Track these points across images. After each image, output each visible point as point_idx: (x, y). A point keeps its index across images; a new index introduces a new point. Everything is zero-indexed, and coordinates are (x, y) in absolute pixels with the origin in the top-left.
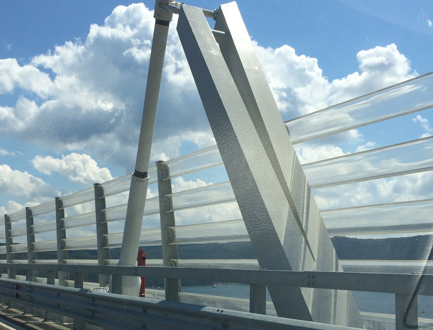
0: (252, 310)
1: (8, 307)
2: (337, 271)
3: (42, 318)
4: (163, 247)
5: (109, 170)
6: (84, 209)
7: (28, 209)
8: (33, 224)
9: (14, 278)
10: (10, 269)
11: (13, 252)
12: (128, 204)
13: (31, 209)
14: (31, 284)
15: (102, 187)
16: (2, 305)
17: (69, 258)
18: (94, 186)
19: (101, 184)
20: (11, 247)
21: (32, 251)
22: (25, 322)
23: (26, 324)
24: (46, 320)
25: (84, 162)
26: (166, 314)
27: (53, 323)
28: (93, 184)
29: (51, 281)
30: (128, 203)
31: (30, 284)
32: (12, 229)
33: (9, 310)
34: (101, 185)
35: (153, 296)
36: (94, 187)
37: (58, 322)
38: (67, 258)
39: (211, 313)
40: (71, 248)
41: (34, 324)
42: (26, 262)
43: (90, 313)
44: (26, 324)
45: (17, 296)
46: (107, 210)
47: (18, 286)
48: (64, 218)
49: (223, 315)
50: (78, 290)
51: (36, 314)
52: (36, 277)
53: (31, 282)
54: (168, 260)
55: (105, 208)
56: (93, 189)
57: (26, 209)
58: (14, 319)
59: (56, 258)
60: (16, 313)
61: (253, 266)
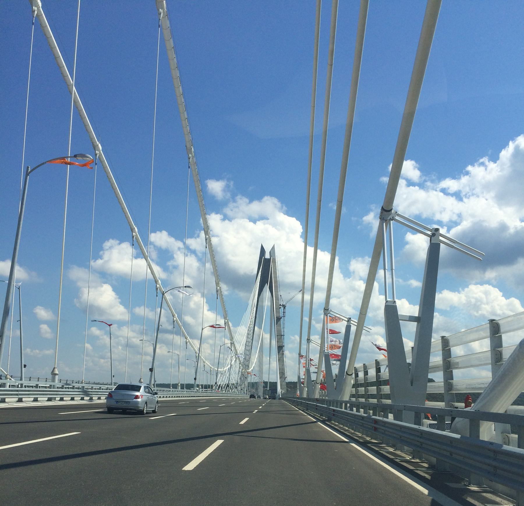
0: (356, 412)
2: (424, 406)
5: (518, 300)
6: (481, 346)
7: (494, 322)
8: (380, 372)
10: (414, 413)
12: (491, 350)
14: (383, 420)
16: (420, 463)
17: (457, 402)
19: (497, 320)
20: (380, 388)
21: (451, 392)
23: (415, 471)
24: (343, 426)
25: (486, 293)
26: (385, 424)
27: (477, 488)
28: (488, 320)
29: (358, 411)
30: (490, 350)
31: (419, 428)
32: (369, 374)
33: (469, 489)
34: (498, 321)
37: (486, 488)
38: (455, 402)
40: (461, 391)
41: (385, 452)
42: (441, 405)
43: (448, 454)
44: (415, 471)
46: (504, 349)
50: (365, 415)
51: (486, 488)
53: (420, 426)
55: (450, 358)
58: (402, 463)
60: (348, 432)
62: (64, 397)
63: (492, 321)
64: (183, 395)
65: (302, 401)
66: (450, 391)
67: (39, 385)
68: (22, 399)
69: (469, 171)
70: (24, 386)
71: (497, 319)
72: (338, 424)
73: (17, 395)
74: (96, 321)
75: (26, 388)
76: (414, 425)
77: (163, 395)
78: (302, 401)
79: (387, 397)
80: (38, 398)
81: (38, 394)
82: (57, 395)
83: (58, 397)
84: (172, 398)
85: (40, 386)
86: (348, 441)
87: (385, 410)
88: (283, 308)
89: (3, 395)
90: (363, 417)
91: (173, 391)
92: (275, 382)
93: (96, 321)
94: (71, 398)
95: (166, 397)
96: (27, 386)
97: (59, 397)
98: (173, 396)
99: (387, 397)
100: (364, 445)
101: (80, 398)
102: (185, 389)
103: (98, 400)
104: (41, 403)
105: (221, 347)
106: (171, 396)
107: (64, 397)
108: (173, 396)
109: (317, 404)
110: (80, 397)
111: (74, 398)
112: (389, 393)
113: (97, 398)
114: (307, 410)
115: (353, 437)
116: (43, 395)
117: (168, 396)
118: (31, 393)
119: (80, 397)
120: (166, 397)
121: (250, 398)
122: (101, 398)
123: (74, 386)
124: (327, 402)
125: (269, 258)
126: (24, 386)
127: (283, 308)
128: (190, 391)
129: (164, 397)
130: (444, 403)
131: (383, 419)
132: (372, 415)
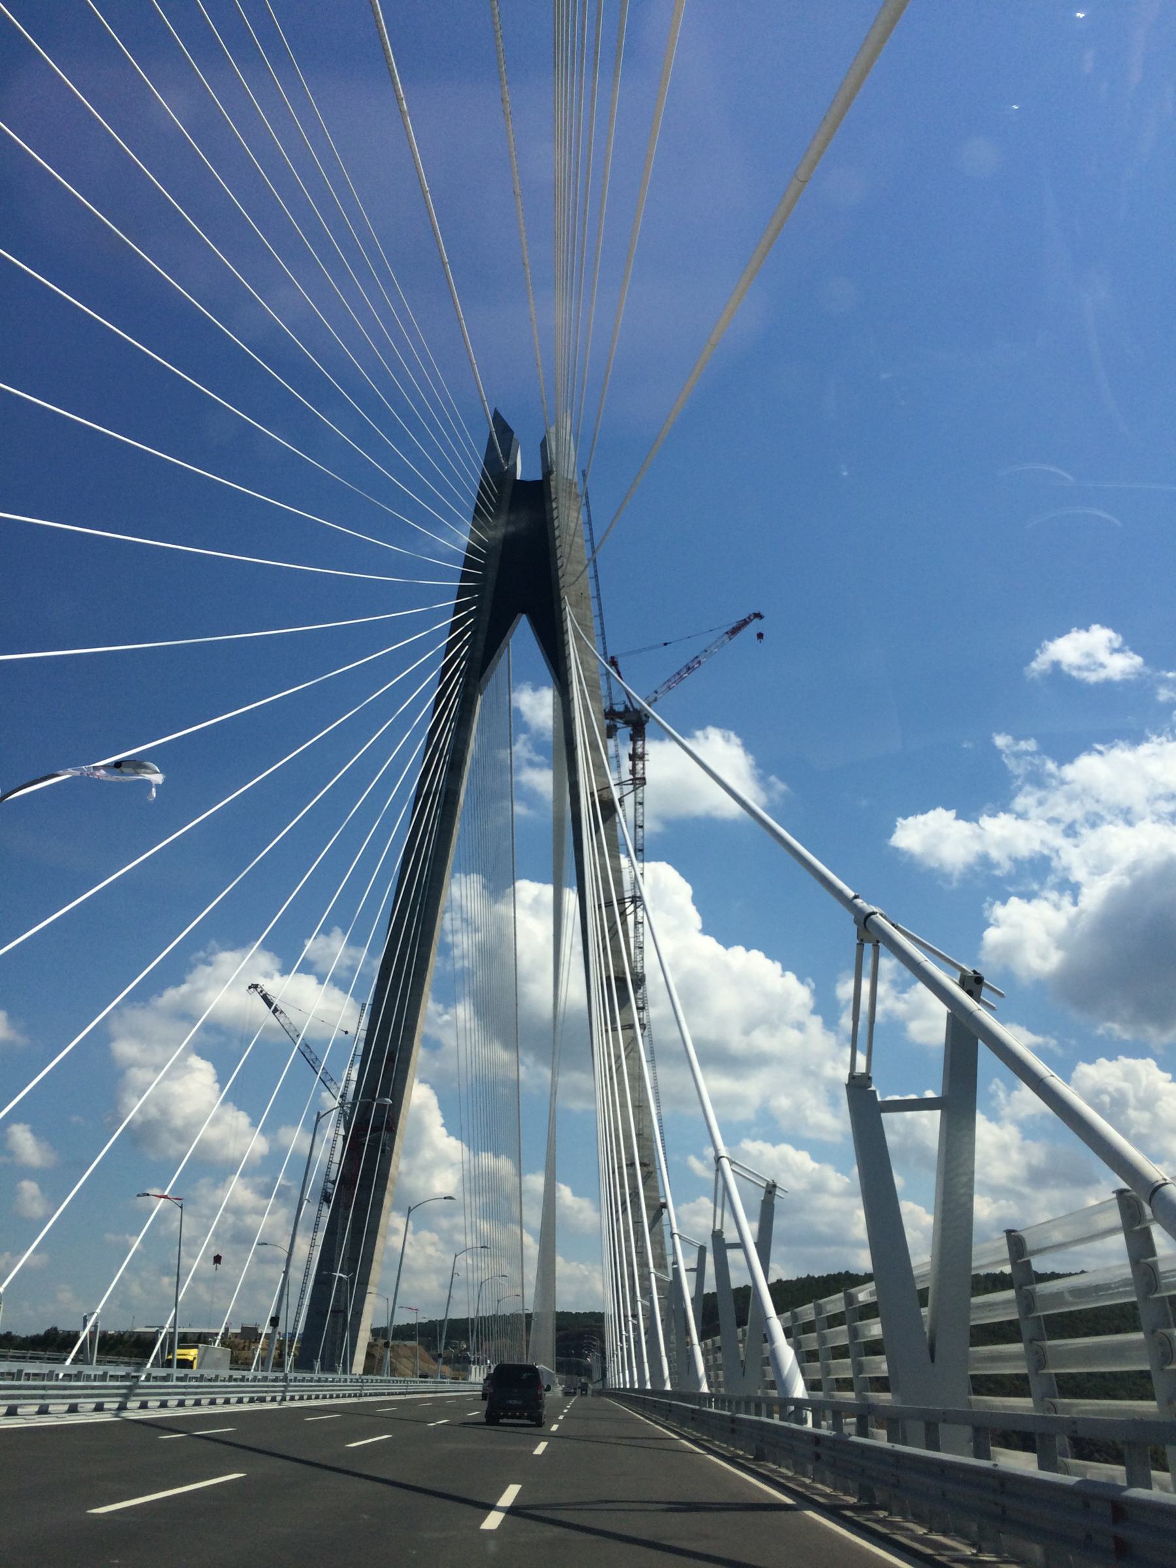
0: (889, 1441)
1: (975, 1551)
3: (925, 1527)
4: (854, 1381)
7: (1013, 1234)
9: (988, 1457)
10: (922, 1424)
11: (869, 1373)
13: (1022, 1234)
15: (1022, 1237)
18: (1114, 1195)
19: (1020, 1231)
22: (888, 1532)
25: (1129, 1075)
28: (1113, 1192)
32: (1158, 1255)
35: (1036, 1465)
36: (1117, 1198)
39: (887, 1449)
42: (1022, 1404)
44: (890, 1535)
45: (655, 1407)
47: (1007, 1482)
48: (1155, 1258)
49: (894, 1450)
52: (1064, 1457)
54: (858, 1394)
56: (1004, 1241)
57: (1007, 1236)
59: (1149, 1396)
61: (851, 1399)
62: (150, 1400)
63: (1009, 1232)
64: (333, 1390)
65: (673, 1402)
66: (1042, 1369)
67: (189, 1376)
68: (166, 1401)
69: (1112, 747)
70: (175, 1378)
71: (1018, 1230)
72: (886, 1514)
73: (63, 1397)
74: (266, 1244)
75: (28, 1380)
76: (974, 1459)
77: (197, 1397)
78: (673, 1402)
79: (881, 1384)
80: (50, 1406)
81: (79, 1396)
82: (266, 1392)
83: (53, 1404)
84: (337, 1400)
85: (27, 1374)
86: (794, 1503)
87: (866, 1416)
88: (629, 729)
89: (7, 1399)
90: (817, 1440)
91: (352, 1379)
92: (582, 1312)
93: (266, 1244)
94: (9, 1407)
95: (308, 1399)
96: (33, 1374)
97: (117, 1402)
98: (311, 1396)
99: (881, 1384)
100: (833, 1511)
101: (66, 1408)
102: (270, 1372)
103: (141, 1410)
104: (86, 1415)
105: (458, 1257)
106: (334, 1394)
107: (150, 1400)
108: (311, 1396)
109: (697, 1407)
110: (64, 1404)
111: (103, 1405)
112: (887, 1375)
113: (158, 1404)
114: (754, 1459)
115: (812, 1496)
116: (32, 1398)
117: (314, 1394)
118: (170, 1390)
119: (64, 1404)
120: (308, 1399)
121: (492, 1419)
122: (150, 1404)
123: (202, 1376)
124: (730, 1402)
125: (539, 477)
126: (175, 1378)
127: (629, 729)
128: (393, 1381)
129: (311, 1399)
130: (1154, 1403)
131: (893, 1446)
132: (1125, 1484)
